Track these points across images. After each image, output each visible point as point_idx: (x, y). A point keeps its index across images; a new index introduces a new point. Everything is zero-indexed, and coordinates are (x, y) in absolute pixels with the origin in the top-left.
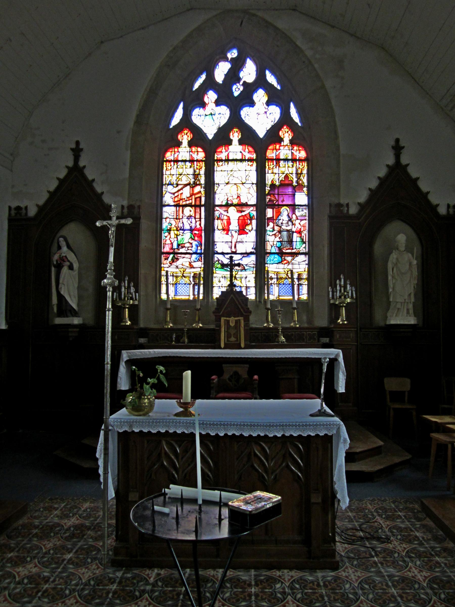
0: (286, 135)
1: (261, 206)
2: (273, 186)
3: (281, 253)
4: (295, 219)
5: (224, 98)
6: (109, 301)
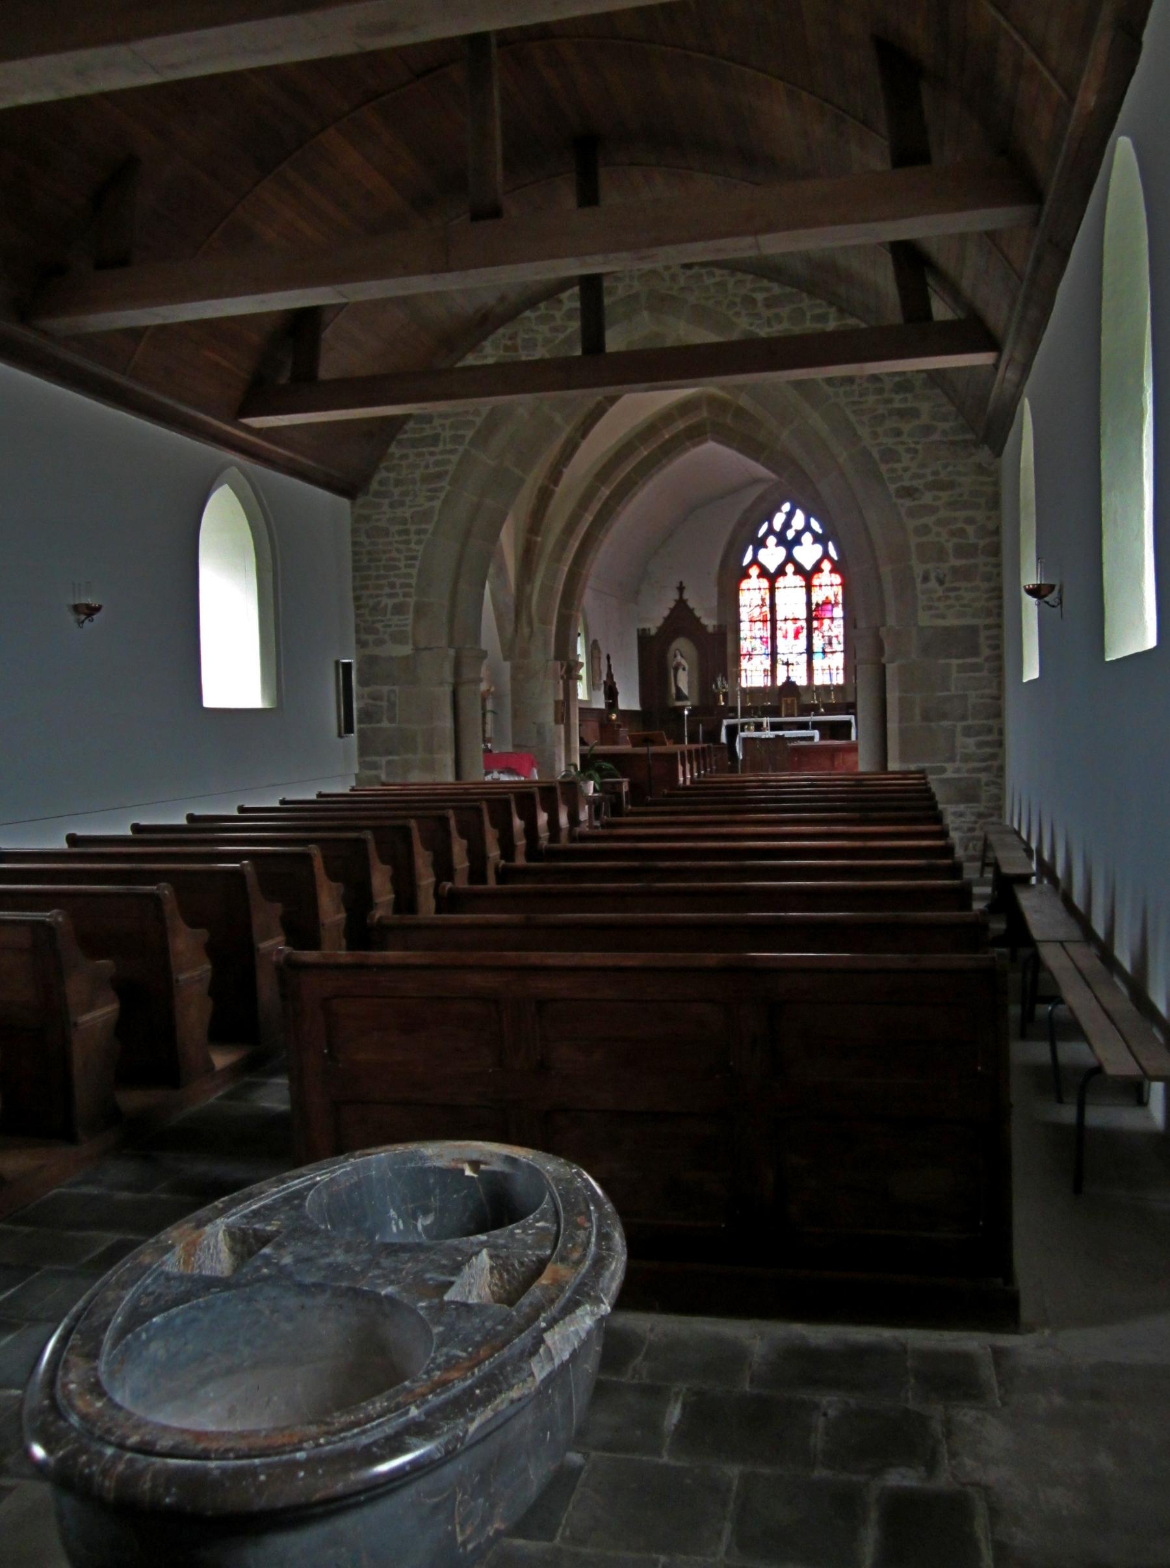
0: (826, 566)
1: (809, 620)
2: (817, 605)
3: (824, 652)
4: (834, 628)
5: (782, 540)
6: (115, 1272)
